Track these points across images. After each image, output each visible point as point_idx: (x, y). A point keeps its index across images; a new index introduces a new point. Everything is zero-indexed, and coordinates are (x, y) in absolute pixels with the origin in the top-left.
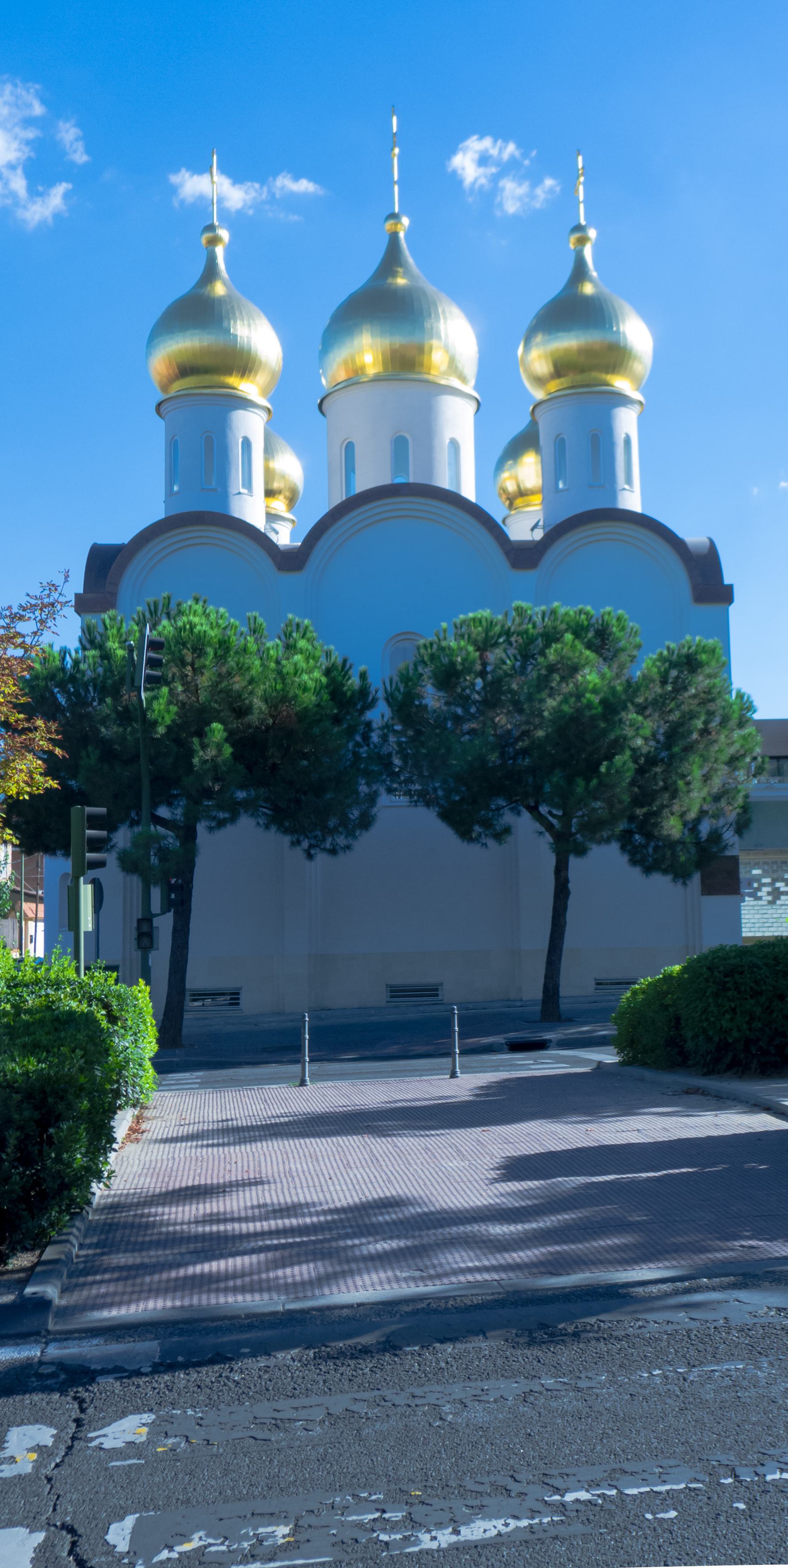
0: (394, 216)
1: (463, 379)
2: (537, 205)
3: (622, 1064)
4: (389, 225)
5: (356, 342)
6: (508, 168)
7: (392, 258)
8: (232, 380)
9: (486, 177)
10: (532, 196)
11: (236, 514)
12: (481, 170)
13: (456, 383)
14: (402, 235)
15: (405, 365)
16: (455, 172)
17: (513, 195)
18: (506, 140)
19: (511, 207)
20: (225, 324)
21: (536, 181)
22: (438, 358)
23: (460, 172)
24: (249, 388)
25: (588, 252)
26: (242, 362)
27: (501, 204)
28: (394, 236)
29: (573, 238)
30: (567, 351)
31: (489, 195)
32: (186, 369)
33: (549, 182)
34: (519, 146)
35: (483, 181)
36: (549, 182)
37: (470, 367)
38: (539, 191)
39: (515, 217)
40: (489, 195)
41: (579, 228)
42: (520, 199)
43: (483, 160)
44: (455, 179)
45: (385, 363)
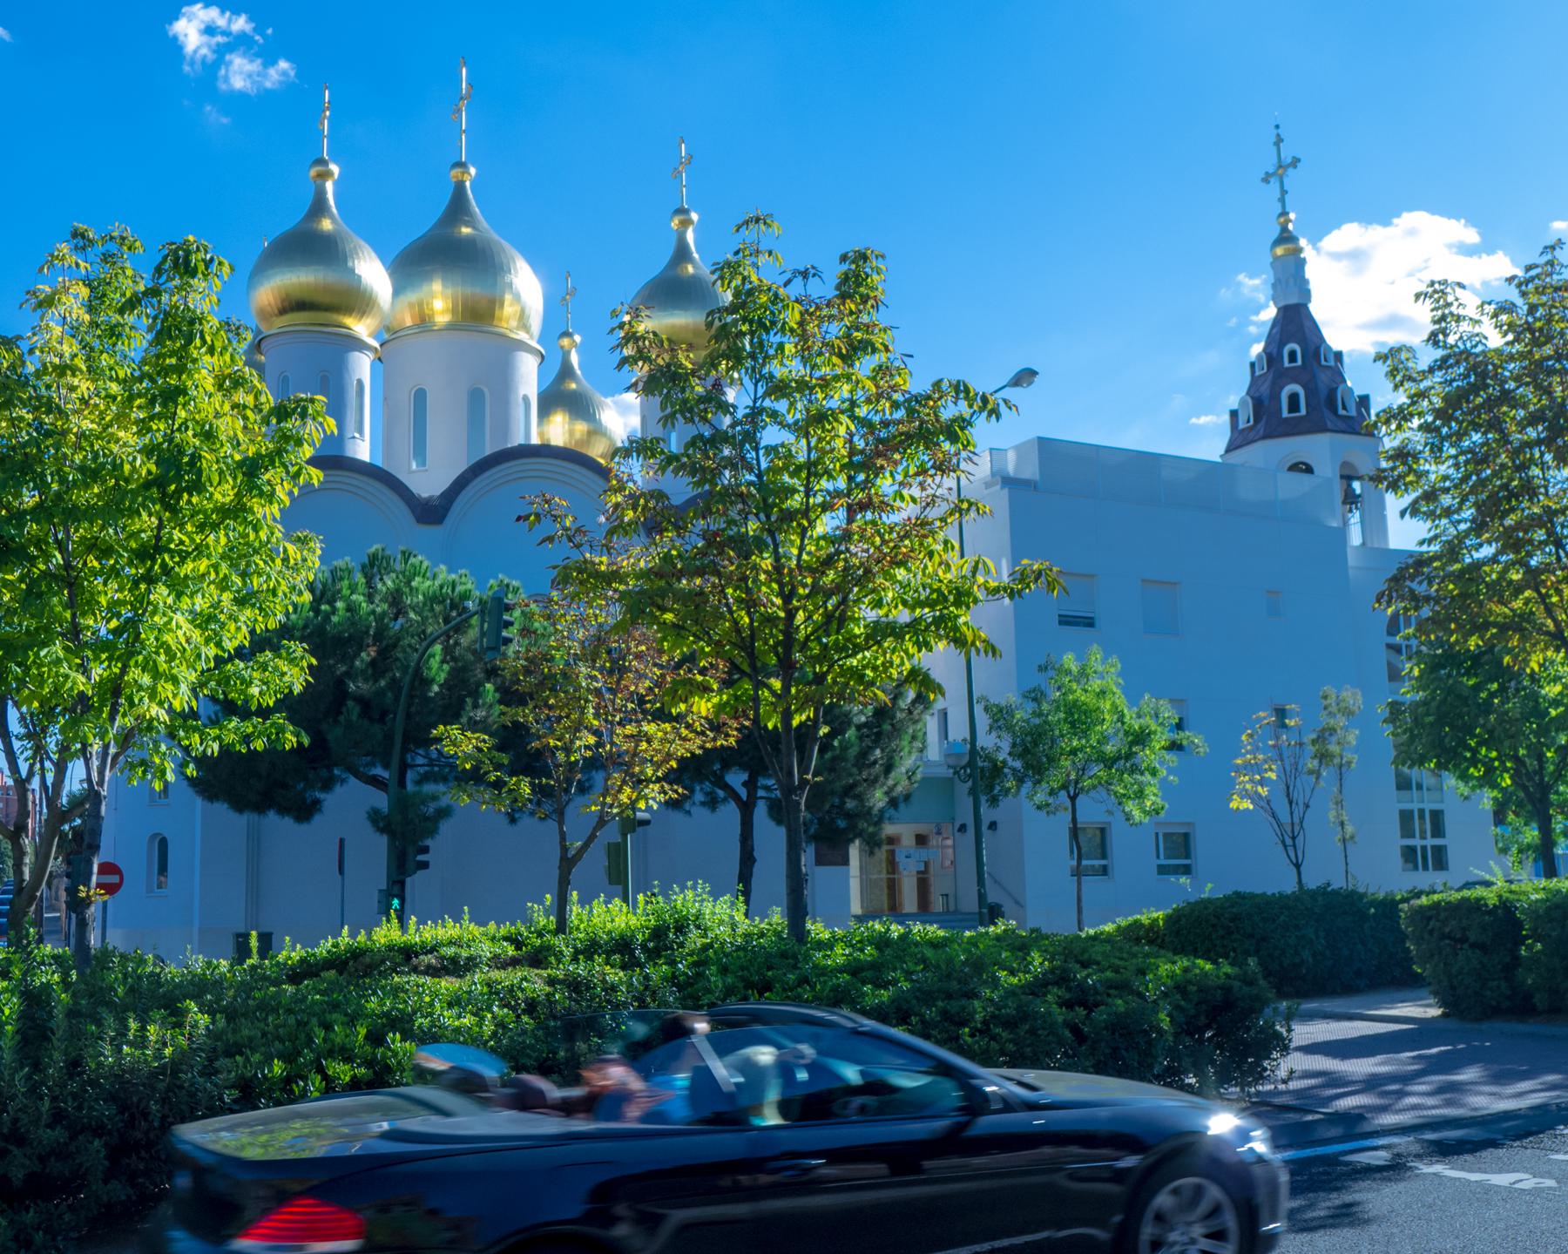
0: (460, 164)
1: (531, 337)
2: (268, 85)
3: (1444, 1015)
4: (456, 172)
5: (425, 288)
6: (239, 43)
7: (458, 207)
8: (349, 321)
9: (209, 47)
10: (264, 75)
11: (349, 454)
12: (205, 38)
13: (522, 336)
14: (468, 184)
15: (477, 316)
16: (175, 38)
17: (240, 73)
18: (236, 12)
19: (238, 83)
20: (350, 264)
21: (270, 61)
22: (509, 309)
23: (182, 38)
24: (361, 328)
25: (690, 236)
26: (356, 300)
27: (226, 79)
28: (460, 186)
29: (675, 224)
30: (673, 326)
31: (213, 67)
32: (296, 305)
33: (283, 65)
34: (250, 19)
35: (204, 51)
36: (283, 65)
37: (536, 323)
38: (272, 72)
39: (242, 95)
40: (213, 67)
41: (681, 211)
42: (250, 76)
43: (209, 30)
44: (175, 45)
45: (454, 311)
